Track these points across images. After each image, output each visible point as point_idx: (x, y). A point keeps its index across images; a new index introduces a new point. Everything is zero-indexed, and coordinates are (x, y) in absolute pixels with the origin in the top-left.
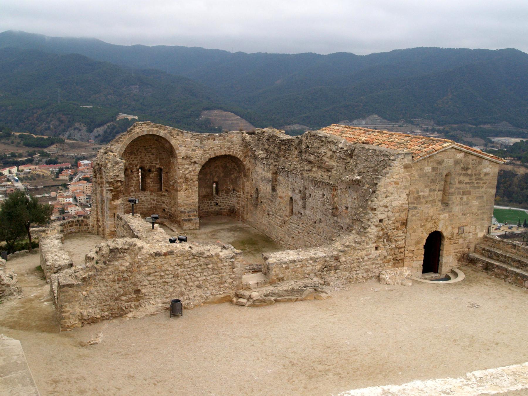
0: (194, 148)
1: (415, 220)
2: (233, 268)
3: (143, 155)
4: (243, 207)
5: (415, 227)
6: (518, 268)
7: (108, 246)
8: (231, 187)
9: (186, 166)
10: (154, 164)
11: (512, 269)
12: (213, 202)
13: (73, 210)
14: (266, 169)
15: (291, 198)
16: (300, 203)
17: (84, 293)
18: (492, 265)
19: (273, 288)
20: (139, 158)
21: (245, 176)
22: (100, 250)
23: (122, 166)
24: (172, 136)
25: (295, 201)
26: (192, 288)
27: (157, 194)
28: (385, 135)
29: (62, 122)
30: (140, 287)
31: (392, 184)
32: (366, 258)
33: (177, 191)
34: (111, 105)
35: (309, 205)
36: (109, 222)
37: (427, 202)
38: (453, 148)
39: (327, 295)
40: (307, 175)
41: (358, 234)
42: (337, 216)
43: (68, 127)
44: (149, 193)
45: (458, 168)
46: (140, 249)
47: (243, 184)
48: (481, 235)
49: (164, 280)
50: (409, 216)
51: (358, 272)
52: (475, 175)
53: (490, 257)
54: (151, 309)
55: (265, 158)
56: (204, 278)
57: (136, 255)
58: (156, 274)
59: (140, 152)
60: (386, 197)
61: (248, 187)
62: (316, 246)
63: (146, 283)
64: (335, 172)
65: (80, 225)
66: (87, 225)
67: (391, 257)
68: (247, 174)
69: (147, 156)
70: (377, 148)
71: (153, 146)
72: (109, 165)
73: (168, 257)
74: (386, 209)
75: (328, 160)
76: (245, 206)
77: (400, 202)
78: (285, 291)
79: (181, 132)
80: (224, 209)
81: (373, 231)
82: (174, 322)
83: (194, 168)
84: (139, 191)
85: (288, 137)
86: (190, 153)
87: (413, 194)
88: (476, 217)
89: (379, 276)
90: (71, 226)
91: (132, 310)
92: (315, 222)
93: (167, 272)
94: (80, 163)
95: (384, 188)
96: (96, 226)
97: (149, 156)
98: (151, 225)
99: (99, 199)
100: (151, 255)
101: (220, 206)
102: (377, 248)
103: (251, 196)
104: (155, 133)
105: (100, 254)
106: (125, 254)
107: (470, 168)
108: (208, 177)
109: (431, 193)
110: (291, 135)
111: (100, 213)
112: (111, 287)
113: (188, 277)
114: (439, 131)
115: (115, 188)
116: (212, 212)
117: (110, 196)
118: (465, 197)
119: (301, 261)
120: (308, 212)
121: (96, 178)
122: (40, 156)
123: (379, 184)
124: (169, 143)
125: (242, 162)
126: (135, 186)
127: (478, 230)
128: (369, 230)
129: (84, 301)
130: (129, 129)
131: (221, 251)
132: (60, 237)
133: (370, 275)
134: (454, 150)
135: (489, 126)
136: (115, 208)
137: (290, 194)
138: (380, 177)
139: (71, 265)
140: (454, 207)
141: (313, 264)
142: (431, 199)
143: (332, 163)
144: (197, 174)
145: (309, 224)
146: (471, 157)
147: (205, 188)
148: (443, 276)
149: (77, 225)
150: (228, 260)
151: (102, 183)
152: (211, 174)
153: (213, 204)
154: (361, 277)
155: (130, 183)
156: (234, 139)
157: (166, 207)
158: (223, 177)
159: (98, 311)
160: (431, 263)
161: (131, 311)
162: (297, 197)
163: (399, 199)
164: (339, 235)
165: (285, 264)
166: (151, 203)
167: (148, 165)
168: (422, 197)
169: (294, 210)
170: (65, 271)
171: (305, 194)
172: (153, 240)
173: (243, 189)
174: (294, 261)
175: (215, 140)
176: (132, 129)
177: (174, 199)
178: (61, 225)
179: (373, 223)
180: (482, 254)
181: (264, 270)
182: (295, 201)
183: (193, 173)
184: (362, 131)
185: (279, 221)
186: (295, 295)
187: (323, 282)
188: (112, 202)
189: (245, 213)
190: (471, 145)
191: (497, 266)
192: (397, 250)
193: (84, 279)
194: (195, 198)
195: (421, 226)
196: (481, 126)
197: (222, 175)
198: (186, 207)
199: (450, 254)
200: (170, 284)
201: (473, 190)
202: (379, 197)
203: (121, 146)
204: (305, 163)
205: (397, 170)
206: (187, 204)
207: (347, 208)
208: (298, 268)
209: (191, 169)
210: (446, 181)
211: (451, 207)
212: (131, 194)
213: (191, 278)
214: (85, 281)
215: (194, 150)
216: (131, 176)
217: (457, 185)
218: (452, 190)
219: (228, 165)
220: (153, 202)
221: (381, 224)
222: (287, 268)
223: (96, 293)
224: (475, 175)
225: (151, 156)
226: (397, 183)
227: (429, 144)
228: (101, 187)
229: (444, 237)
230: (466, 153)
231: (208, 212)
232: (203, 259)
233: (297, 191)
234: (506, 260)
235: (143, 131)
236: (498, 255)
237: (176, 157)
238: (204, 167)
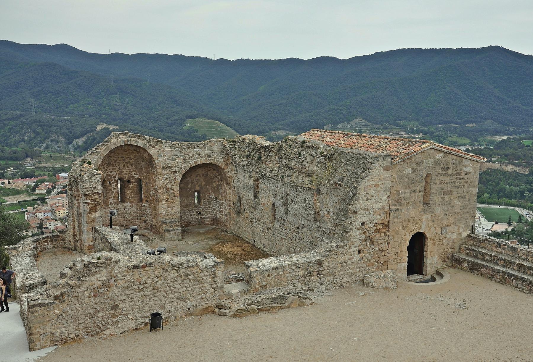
0: (174, 157)
1: (397, 222)
2: (214, 278)
5: (397, 229)
6: (504, 266)
7: (83, 261)
9: (166, 176)
11: (514, 273)
13: (51, 225)
14: (247, 176)
15: (274, 204)
16: (283, 209)
17: (56, 311)
18: (478, 264)
19: (255, 297)
20: (117, 169)
21: (227, 183)
22: (74, 265)
23: (99, 178)
24: (150, 145)
25: (278, 207)
26: (173, 300)
27: (137, 205)
28: (364, 138)
29: (38, 134)
30: (117, 303)
31: (372, 187)
32: (349, 262)
33: (157, 201)
34: (90, 116)
35: (291, 211)
36: (87, 236)
37: (408, 203)
38: (432, 148)
39: (311, 301)
40: (288, 181)
41: (340, 238)
42: (319, 221)
43: (45, 139)
44: (129, 204)
45: (438, 168)
46: (116, 262)
48: (465, 234)
49: (143, 293)
50: (391, 218)
51: (342, 276)
52: (456, 174)
53: (476, 257)
54: (131, 324)
55: (247, 165)
56: (185, 289)
57: (113, 268)
58: (135, 287)
60: (367, 200)
61: (231, 195)
62: (300, 252)
63: (124, 297)
64: (315, 177)
65: (56, 241)
66: (63, 240)
67: (375, 260)
70: (357, 151)
71: (132, 157)
72: (86, 177)
73: (146, 269)
74: (367, 212)
75: (309, 164)
77: (381, 204)
78: (268, 299)
79: (160, 141)
80: (207, 218)
81: (356, 234)
82: (154, 335)
84: (118, 202)
85: (268, 143)
86: (170, 163)
87: (394, 196)
88: (459, 217)
89: (363, 280)
90: (45, 242)
91: (109, 326)
92: (298, 228)
93: (146, 285)
94: (59, 176)
95: (364, 190)
96: (72, 240)
97: (128, 167)
98: (130, 237)
99: (76, 212)
100: (128, 267)
101: (202, 215)
102: (359, 252)
103: (234, 204)
104: (133, 143)
105: (74, 269)
106: (101, 268)
107: (450, 168)
108: (190, 186)
109: (413, 195)
110: (271, 141)
111: (77, 228)
112: (86, 303)
113: (168, 289)
114: (423, 132)
115: (93, 201)
117: (87, 208)
118: (446, 198)
119: (283, 267)
120: (290, 218)
121: (72, 191)
122: (14, 169)
123: (359, 187)
124: (148, 152)
125: (223, 170)
126: (114, 197)
127: (461, 230)
128: (351, 233)
129: (56, 320)
130: (105, 140)
131: (202, 261)
132: (33, 254)
133: (354, 279)
134: (433, 150)
135: (474, 125)
136: (93, 221)
137: (272, 200)
138: (360, 180)
139: (45, 283)
140: (436, 208)
141: (295, 270)
142: (413, 200)
143: (314, 168)
144: (178, 183)
145: (292, 230)
146: (451, 157)
148: (428, 277)
149: (52, 241)
150: (209, 270)
151: (79, 196)
152: (192, 183)
154: (345, 282)
155: (108, 195)
156: (215, 147)
158: (204, 185)
159: (72, 330)
160: (416, 266)
161: (107, 329)
162: (279, 203)
163: (380, 201)
164: (322, 240)
165: (267, 271)
168: (402, 198)
169: (276, 216)
170: (37, 290)
171: (287, 200)
172: (130, 253)
173: (225, 197)
174: (277, 268)
176: (108, 140)
177: (154, 209)
178: (34, 241)
179: (355, 227)
180: (467, 254)
181: (245, 279)
183: (173, 182)
184: (342, 135)
185: (262, 227)
186: (278, 304)
187: (307, 289)
188: (90, 215)
189: (228, 220)
190: (454, 144)
191: (483, 265)
192: (380, 253)
193: (56, 297)
194: (176, 208)
195: (404, 228)
196: (467, 125)
197: (203, 183)
198: (167, 217)
199: (434, 255)
200: (150, 296)
201: (454, 190)
202: (361, 201)
203: (97, 157)
204: (286, 169)
205: (377, 171)
207: (329, 212)
208: (281, 275)
210: (426, 182)
211: (432, 207)
212: (110, 206)
213: (171, 290)
214: (57, 299)
215: (173, 159)
216: (109, 188)
217: (438, 186)
218: (433, 191)
219: (209, 173)
221: (363, 227)
222: (269, 275)
223: (70, 312)
224: (456, 174)
225: (130, 166)
226: (376, 186)
227: (409, 146)
228: (78, 200)
229: (427, 238)
230: (445, 152)
232: (183, 270)
233: (279, 197)
234: (494, 260)
235: (121, 141)
236: (483, 254)
237: (156, 167)
238: (184, 176)
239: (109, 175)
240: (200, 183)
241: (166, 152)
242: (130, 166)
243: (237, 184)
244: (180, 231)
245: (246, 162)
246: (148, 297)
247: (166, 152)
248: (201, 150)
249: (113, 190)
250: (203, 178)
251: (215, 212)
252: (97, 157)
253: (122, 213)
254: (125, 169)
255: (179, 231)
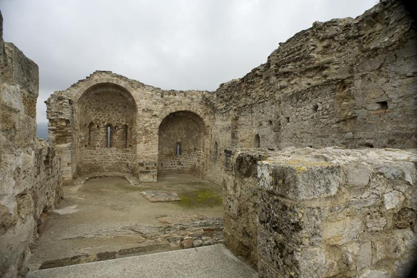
3: (111, 113)
4: (203, 164)
8: (192, 147)
9: (147, 119)
10: (121, 122)
12: (176, 161)
16: (272, 137)
20: (106, 115)
21: (206, 134)
24: (132, 87)
33: (136, 143)
44: (115, 149)
47: (204, 142)
59: (108, 109)
61: (207, 143)
68: (207, 131)
69: (115, 114)
71: (120, 104)
75: (320, 56)
76: (205, 162)
80: (186, 168)
83: (154, 122)
97: (117, 115)
101: (182, 165)
103: (210, 152)
104: (115, 82)
108: (172, 138)
116: (175, 171)
126: (102, 141)
137: (255, 131)
144: (157, 127)
147: (169, 147)
152: (175, 135)
153: (176, 163)
157: (129, 162)
158: (186, 138)
166: (117, 159)
167: (115, 123)
173: (203, 147)
175: (176, 95)
182: (263, 137)
183: (153, 126)
197: (185, 136)
198: (145, 160)
203: (77, 91)
206: (146, 157)
209: (151, 122)
212: (97, 148)
216: (97, 131)
219: (190, 127)
220: (118, 158)
231: (172, 170)
233: (265, 124)
235: (103, 79)
239: (98, 120)
240: (181, 136)
241: (147, 95)
242: (118, 114)
243: (214, 131)
244: (156, 173)
245: (225, 105)
246: (342, 208)
247: (147, 95)
248: (182, 97)
249: (101, 134)
250: (184, 131)
251: (193, 162)
252: (77, 91)
253: (108, 156)
254: (113, 117)
255: (154, 173)
